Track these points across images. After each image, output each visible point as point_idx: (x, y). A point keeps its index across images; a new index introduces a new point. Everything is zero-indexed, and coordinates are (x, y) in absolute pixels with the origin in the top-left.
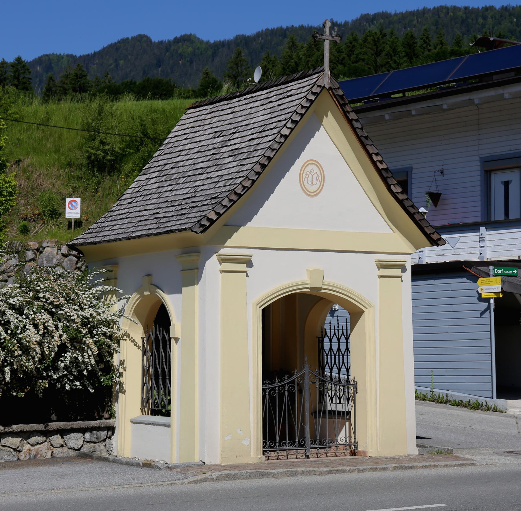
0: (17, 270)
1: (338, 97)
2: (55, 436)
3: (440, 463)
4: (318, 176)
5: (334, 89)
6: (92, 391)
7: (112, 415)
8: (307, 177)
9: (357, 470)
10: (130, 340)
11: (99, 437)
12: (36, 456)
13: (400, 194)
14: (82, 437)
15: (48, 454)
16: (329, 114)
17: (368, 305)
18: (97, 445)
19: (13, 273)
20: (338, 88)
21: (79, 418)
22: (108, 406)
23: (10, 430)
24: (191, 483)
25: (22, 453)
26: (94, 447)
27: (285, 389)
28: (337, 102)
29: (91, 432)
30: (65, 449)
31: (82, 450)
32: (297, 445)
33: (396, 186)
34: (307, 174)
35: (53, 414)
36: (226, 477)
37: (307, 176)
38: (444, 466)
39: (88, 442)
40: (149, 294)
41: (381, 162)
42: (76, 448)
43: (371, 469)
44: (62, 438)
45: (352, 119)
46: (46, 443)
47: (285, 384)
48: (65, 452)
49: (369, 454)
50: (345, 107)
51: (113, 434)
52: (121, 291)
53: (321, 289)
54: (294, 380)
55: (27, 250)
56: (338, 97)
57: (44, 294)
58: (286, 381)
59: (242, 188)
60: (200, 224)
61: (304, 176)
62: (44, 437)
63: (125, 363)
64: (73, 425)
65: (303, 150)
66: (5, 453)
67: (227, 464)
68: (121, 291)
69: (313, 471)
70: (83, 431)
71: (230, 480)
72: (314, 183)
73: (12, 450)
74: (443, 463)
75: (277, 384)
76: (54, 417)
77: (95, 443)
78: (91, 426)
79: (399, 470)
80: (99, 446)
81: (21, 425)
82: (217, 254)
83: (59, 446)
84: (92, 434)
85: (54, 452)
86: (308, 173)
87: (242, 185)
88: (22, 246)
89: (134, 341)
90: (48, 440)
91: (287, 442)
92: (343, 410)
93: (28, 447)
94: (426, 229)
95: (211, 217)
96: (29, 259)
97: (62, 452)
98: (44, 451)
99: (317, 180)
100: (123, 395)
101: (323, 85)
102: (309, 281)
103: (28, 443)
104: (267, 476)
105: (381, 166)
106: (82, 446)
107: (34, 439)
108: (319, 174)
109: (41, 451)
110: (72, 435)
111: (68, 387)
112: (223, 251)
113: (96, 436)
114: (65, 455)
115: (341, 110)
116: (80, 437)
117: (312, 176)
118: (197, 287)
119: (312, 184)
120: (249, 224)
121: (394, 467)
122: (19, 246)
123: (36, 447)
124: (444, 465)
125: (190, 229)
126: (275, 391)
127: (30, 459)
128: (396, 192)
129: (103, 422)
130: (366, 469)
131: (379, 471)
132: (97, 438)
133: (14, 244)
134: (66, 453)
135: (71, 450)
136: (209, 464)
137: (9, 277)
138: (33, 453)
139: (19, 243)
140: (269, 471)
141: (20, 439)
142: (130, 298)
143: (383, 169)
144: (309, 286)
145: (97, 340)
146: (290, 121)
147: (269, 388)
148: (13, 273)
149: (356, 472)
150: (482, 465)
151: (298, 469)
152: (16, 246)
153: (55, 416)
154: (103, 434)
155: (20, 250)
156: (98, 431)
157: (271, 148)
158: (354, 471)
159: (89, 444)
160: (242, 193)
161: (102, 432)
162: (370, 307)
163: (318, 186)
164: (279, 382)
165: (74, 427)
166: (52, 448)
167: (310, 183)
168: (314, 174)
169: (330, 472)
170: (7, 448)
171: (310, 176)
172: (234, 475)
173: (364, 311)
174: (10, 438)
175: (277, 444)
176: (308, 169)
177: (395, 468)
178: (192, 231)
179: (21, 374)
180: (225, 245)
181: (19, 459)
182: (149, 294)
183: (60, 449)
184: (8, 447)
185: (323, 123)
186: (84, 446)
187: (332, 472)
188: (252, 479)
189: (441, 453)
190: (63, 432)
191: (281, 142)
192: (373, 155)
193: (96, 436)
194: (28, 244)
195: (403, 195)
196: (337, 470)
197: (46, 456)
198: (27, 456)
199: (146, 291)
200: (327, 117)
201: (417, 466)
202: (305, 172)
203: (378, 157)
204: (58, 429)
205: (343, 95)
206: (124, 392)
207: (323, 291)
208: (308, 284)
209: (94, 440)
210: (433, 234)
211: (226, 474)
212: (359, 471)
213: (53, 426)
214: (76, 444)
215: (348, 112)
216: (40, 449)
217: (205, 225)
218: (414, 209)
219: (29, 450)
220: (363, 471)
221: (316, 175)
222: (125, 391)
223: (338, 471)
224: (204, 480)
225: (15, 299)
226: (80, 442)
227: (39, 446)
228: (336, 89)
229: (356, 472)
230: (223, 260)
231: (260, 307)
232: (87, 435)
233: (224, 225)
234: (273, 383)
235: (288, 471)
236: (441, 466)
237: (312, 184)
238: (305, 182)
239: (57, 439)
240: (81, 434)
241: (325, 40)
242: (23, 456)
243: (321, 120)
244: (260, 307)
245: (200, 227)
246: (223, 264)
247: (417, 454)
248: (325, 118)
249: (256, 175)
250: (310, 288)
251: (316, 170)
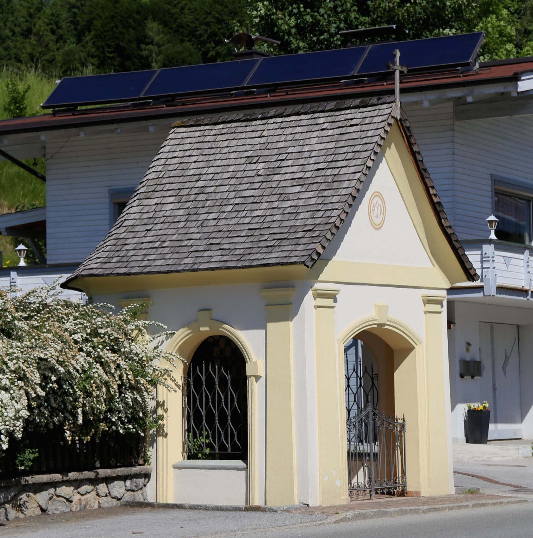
1: (405, 129)
2: (102, 485)
4: (381, 209)
7: (146, 461)
10: (171, 379)
12: (85, 506)
16: (393, 146)
18: (135, 493)
21: (118, 464)
22: (142, 452)
23: (67, 478)
24: (336, 522)
25: (73, 503)
26: (134, 495)
28: (404, 134)
29: (131, 479)
31: (123, 500)
34: (373, 206)
40: (208, 329)
41: (435, 195)
45: (416, 152)
49: (422, 495)
51: (148, 482)
52: (166, 327)
53: (384, 325)
56: (405, 129)
57: (106, 330)
60: (311, 257)
62: (70, 487)
63: (165, 404)
66: (60, 503)
68: (166, 327)
70: (124, 478)
72: (379, 216)
73: (65, 501)
74: (471, 503)
80: (138, 495)
81: (76, 473)
83: (104, 495)
85: (101, 502)
89: (175, 380)
92: (369, 452)
93: (78, 496)
95: (319, 251)
97: (107, 502)
98: (92, 501)
100: (164, 439)
102: (377, 317)
103: (79, 493)
105: (436, 200)
107: (85, 488)
108: (382, 207)
109: (90, 501)
110: (116, 483)
112: (317, 286)
113: (135, 484)
114: (110, 505)
115: (406, 141)
118: (291, 325)
120: (334, 258)
121: (473, 505)
123: (86, 497)
125: (303, 263)
127: (80, 510)
130: (454, 507)
132: (136, 486)
135: (114, 500)
138: (83, 503)
141: (72, 488)
142: (174, 333)
144: (377, 322)
145: (150, 379)
149: (447, 511)
151: (407, 508)
154: (141, 481)
156: (137, 478)
157: (360, 180)
158: (445, 509)
161: (140, 480)
162: (420, 343)
163: (381, 218)
166: (98, 497)
167: (376, 216)
169: (429, 510)
170: (61, 498)
171: (376, 208)
173: (414, 348)
174: (64, 487)
176: (374, 202)
178: (305, 265)
179: (91, 416)
181: (71, 510)
182: (208, 329)
183: (105, 499)
184: (63, 497)
186: (126, 495)
189: (472, 493)
190: (108, 480)
193: (135, 484)
198: (78, 506)
199: (204, 326)
202: (372, 205)
206: (166, 436)
207: (386, 327)
208: (376, 320)
209: (134, 488)
214: (119, 493)
216: (89, 499)
219: (80, 500)
222: (167, 434)
225: (79, 335)
227: (88, 495)
229: (447, 511)
230: (319, 295)
232: (128, 483)
238: (372, 214)
239: (102, 488)
240: (123, 482)
241: (396, 70)
242: (75, 507)
245: (311, 261)
246: (318, 299)
247: (454, 493)
248: (388, 149)
250: (378, 325)
251: (380, 203)
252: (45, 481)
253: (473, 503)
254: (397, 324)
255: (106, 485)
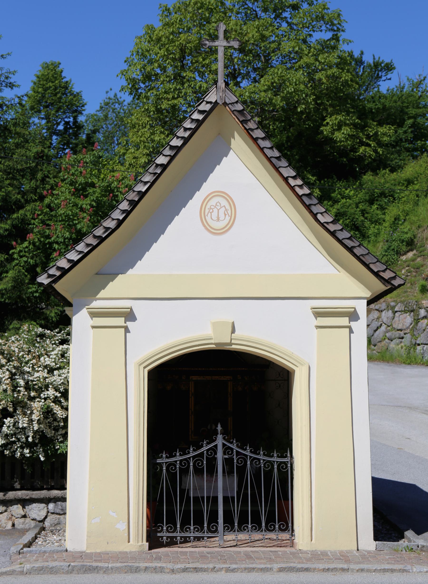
0: (412, 328)
2: (15, 506)
3: (352, 566)
4: (226, 210)
5: (231, 104)
6: (42, 459)
8: (211, 213)
9: (224, 569)
11: (64, 508)
13: (331, 224)
14: (46, 508)
15: (8, 525)
17: (300, 363)
18: (61, 516)
19: (408, 331)
20: (237, 102)
26: (59, 519)
27: (189, 464)
29: (55, 502)
30: (28, 520)
32: (206, 532)
33: (325, 214)
35: (16, 482)
36: (40, 570)
37: (211, 211)
38: (358, 571)
39: (53, 513)
42: (38, 519)
43: (245, 569)
44: (24, 507)
46: (5, 514)
47: (190, 458)
48: (27, 524)
50: (246, 124)
53: (231, 344)
54: (203, 453)
55: (420, 308)
56: (236, 113)
58: (192, 455)
59: (104, 230)
61: (207, 211)
62: (3, 506)
64: (33, 494)
65: (205, 180)
67: (94, 551)
69: (160, 567)
70: (47, 501)
71: (45, 574)
75: (178, 458)
76: (17, 485)
77: (60, 514)
78: (52, 497)
79: (287, 571)
82: (87, 307)
83: (20, 516)
84: (56, 505)
86: (212, 207)
87: (104, 226)
88: (417, 305)
90: (9, 510)
91: (250, 526)
94: (372, 266)
96: (422, 316)
99: (225, 215)
101: (214, 101)
104: (96, 571)
106: (46, 517)
108: (228, 207)
110: (34, 505)
111: (18, 455)
112: (96, 304)
113: (60, 507)
116: (43, 507)
117: (218, 210)
119: (218, 219)
120: (130, 272)
122: (414, 305)
124: (357, 569)
126: (175, 466)
128: (325, 222)
129: (55, 493)
130: (238, 569)
131: (256, 572)
133: (409, 303)
134: (28, 525)
135: (32, 522)
136: (72, 550)
137: (405, 334)
139: (414, 302)
140: (100, 564)
143: (304, 195)
144: (213, 341)
146: (169, 146)
147: (166, 463)
148: (408, 331)
149: (223, 572)
150: (420, 572)
152: (412, 305)
153: (19, 484)
155: (415, 308)
159: (54, 515)
160: (104, 236)
162: (302, 365)
164: (180, 455)
165: (33, 497)
168: (221, 208)
171: (215, 210)
172: (52, 568)
175: (178, 529)
176: (213, 202)
177: (281, 570)
180: (98, 296)
185: (232, 147)
186: (48, 518)
187: (188, 570)
188: (76, 574)
191: (156, 173)
192: (290, 179)
193: (60, 507)
194: (421, 303)
195: (335, 225)
196: (196, 568)
197: (5, 527)
200: (234, 139)
201: (315, 569)
202: (208, 206)
203: (296, 181)
204: (15, 498)
205: (243, 110)
207: (234, 346)
209: (58, 511)
210: (384, 271)
211: (39, 567)
212: (228, 570)
213: (11, 495)
215: (252, 130)
217: (55, 275)
218: (353, 241)
220: (233, 570)
221: (223, 209)
223: (196, 570)
224: (10, 573)
226: (43, 514)
228: (233, 103)
229: (223, 572)
230: (93, 315)
231: (145, 367)
232: (51, 506)
233: (97, 274)
234: (171, 456)
235: (126, 566)
236: (353, 570)
237: (218, 219)
238: (208, 218)
239: (17, 509)
240: (44, 505)
243: (230, 144)
244: (145, 367)
246: (94, 318)
248: (232, 140)
249: (123, 213)
251: (224, 202)
252: (42, 497)
253: (279, 566)
254: (204, 340)
255: (21, 507)
